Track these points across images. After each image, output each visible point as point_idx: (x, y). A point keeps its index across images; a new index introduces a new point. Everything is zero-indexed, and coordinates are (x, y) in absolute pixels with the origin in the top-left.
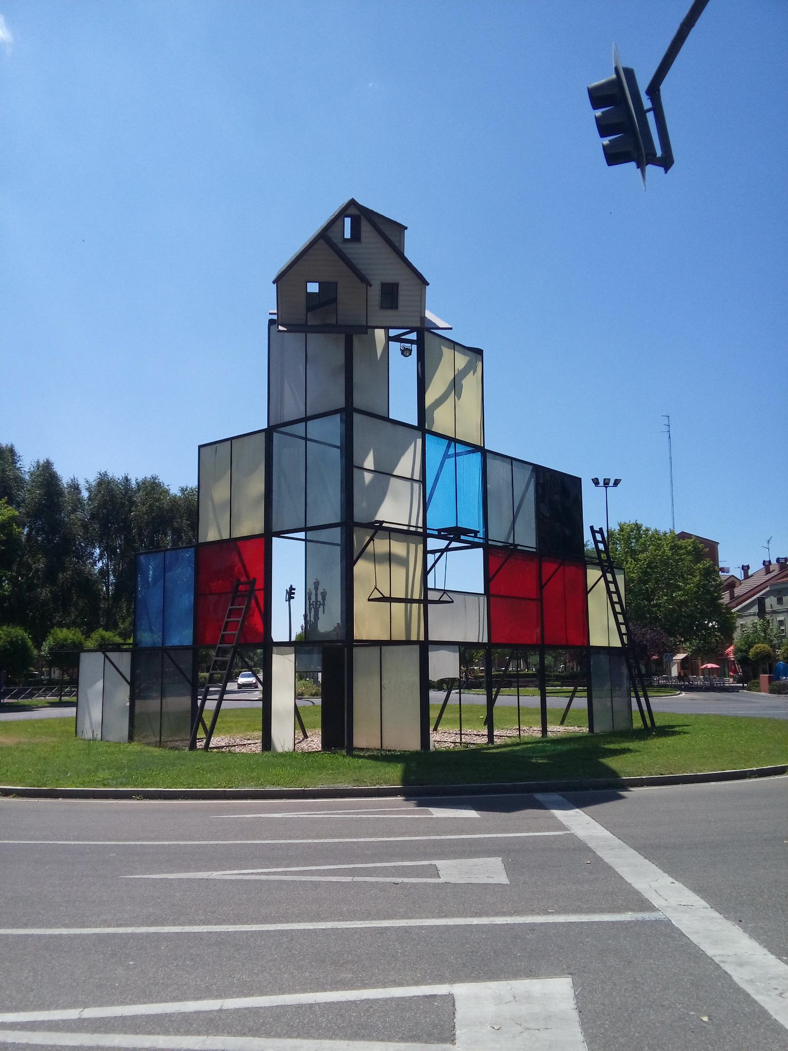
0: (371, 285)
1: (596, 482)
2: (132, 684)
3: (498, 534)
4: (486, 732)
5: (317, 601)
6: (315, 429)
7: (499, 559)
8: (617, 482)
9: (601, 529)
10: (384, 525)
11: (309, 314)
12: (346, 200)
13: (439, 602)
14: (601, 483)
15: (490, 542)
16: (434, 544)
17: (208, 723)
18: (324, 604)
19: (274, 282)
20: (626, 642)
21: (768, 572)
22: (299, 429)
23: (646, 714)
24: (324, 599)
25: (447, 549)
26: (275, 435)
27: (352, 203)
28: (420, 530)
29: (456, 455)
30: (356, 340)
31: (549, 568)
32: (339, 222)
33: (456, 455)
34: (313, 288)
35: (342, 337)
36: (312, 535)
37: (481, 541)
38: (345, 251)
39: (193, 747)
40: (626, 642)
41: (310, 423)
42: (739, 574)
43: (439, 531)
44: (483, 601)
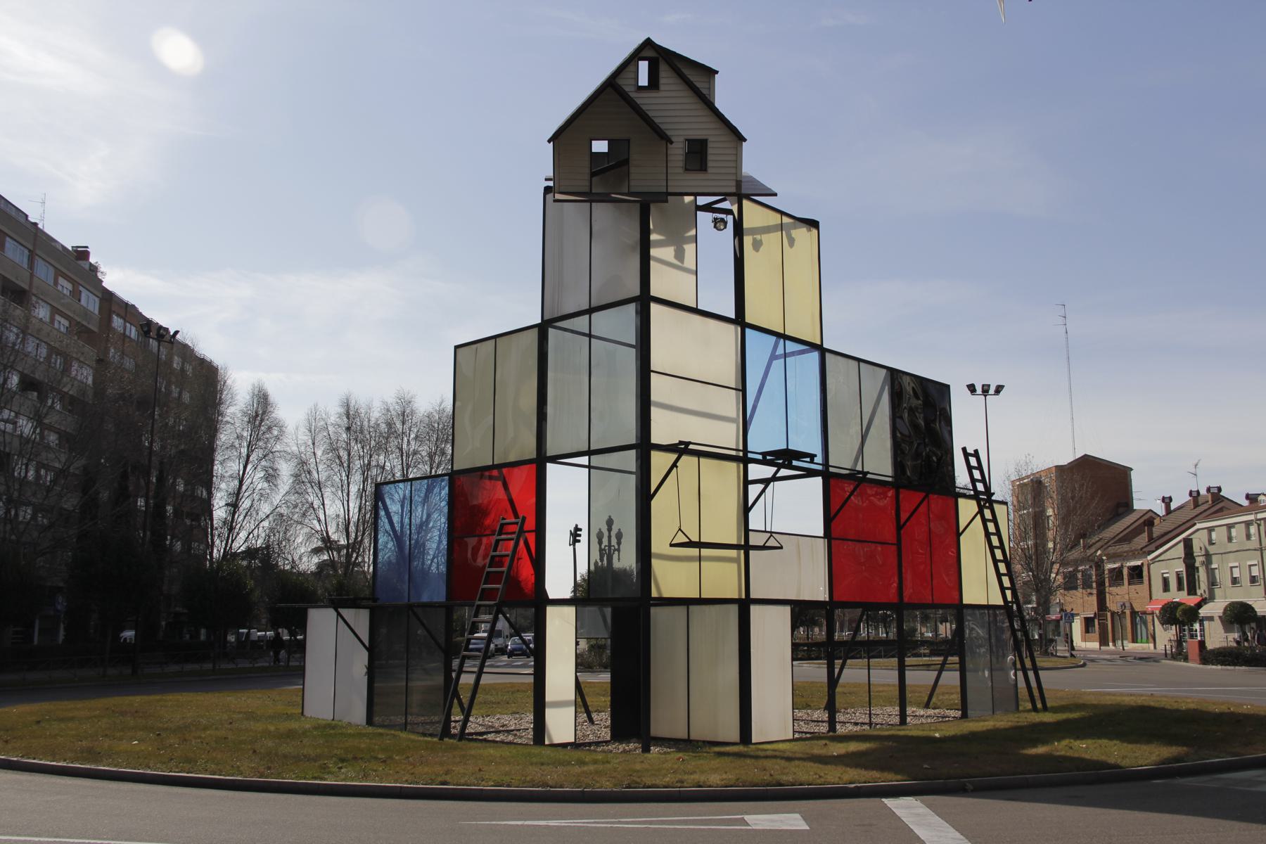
0: (672, 143)
1: (972, 388)
2: (370, 650)
3: (842, 460)
4: (826, 716)
5: (610, 545)
6: (603, 323)
7: (842, 491)
8: (999, 389)
9: (976, 451)
10: (691, 447)
11: (594, 179)
12: (640, 40)
13: (764, 548)
14: (979, 390)
15: (831, 470)
16: (756, 471)
17: (466, 701)
18: (619, 550)
19: (549, 141)
20: (1009, 599)
21: (1196, 505)
22: (581, 323)
23: (1036, 693)
24: (619, 543)
25: (775, 478)
26: (552, 332)
27: (648, 43)
28: (741, 454)
29: (785, 355)
30: (653, 208)
31: (910, 499)
32: (631, 68)
33: (785, 355)
34: (600, 146)
35: (636, 209)
36: (597, 460)
37: (820, 468)
38: (638, 101)
39: (446, 732)
40: (1009, 599)
41: (594, 316)
42: (1160, 509)
43: (764, 454)
44: (822, 545)
